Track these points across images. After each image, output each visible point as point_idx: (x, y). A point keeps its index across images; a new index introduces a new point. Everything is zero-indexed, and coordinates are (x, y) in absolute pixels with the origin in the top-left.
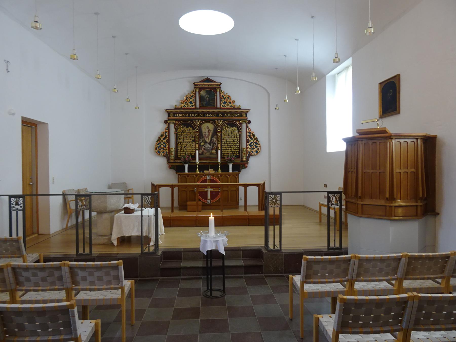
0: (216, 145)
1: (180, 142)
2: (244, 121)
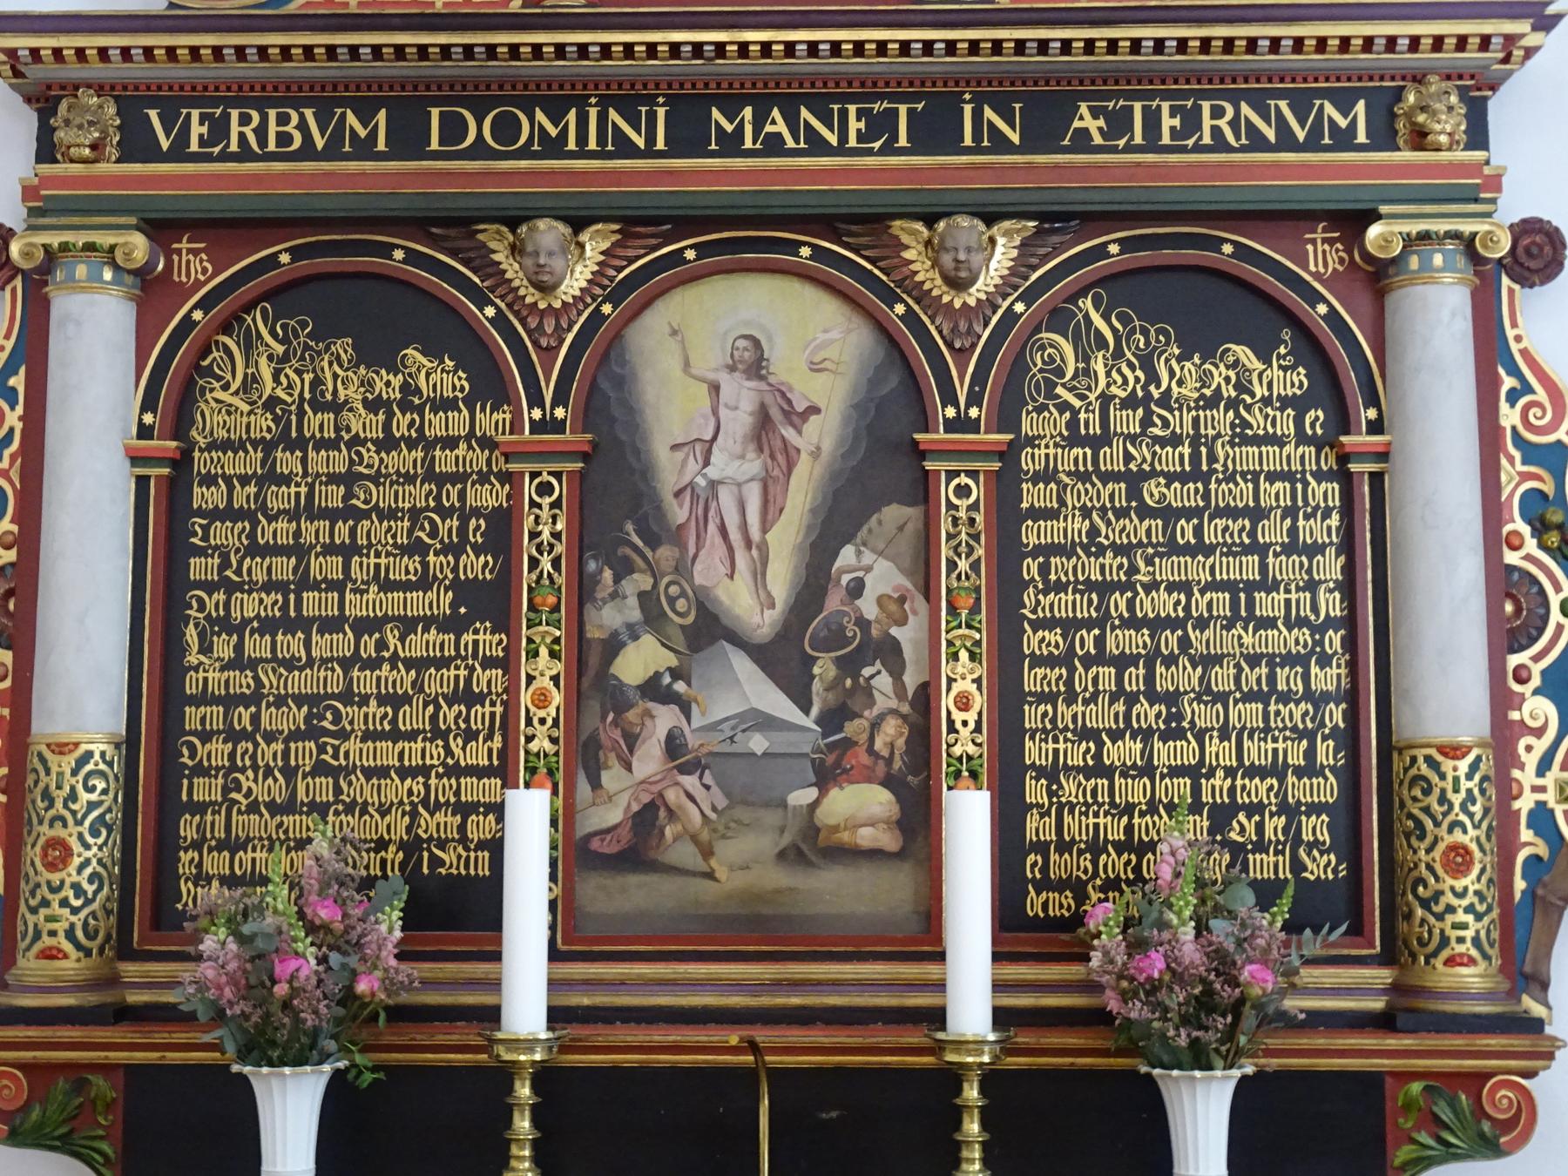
0: (911, 680)
1: (240, 629)
2: (1442, 226)
